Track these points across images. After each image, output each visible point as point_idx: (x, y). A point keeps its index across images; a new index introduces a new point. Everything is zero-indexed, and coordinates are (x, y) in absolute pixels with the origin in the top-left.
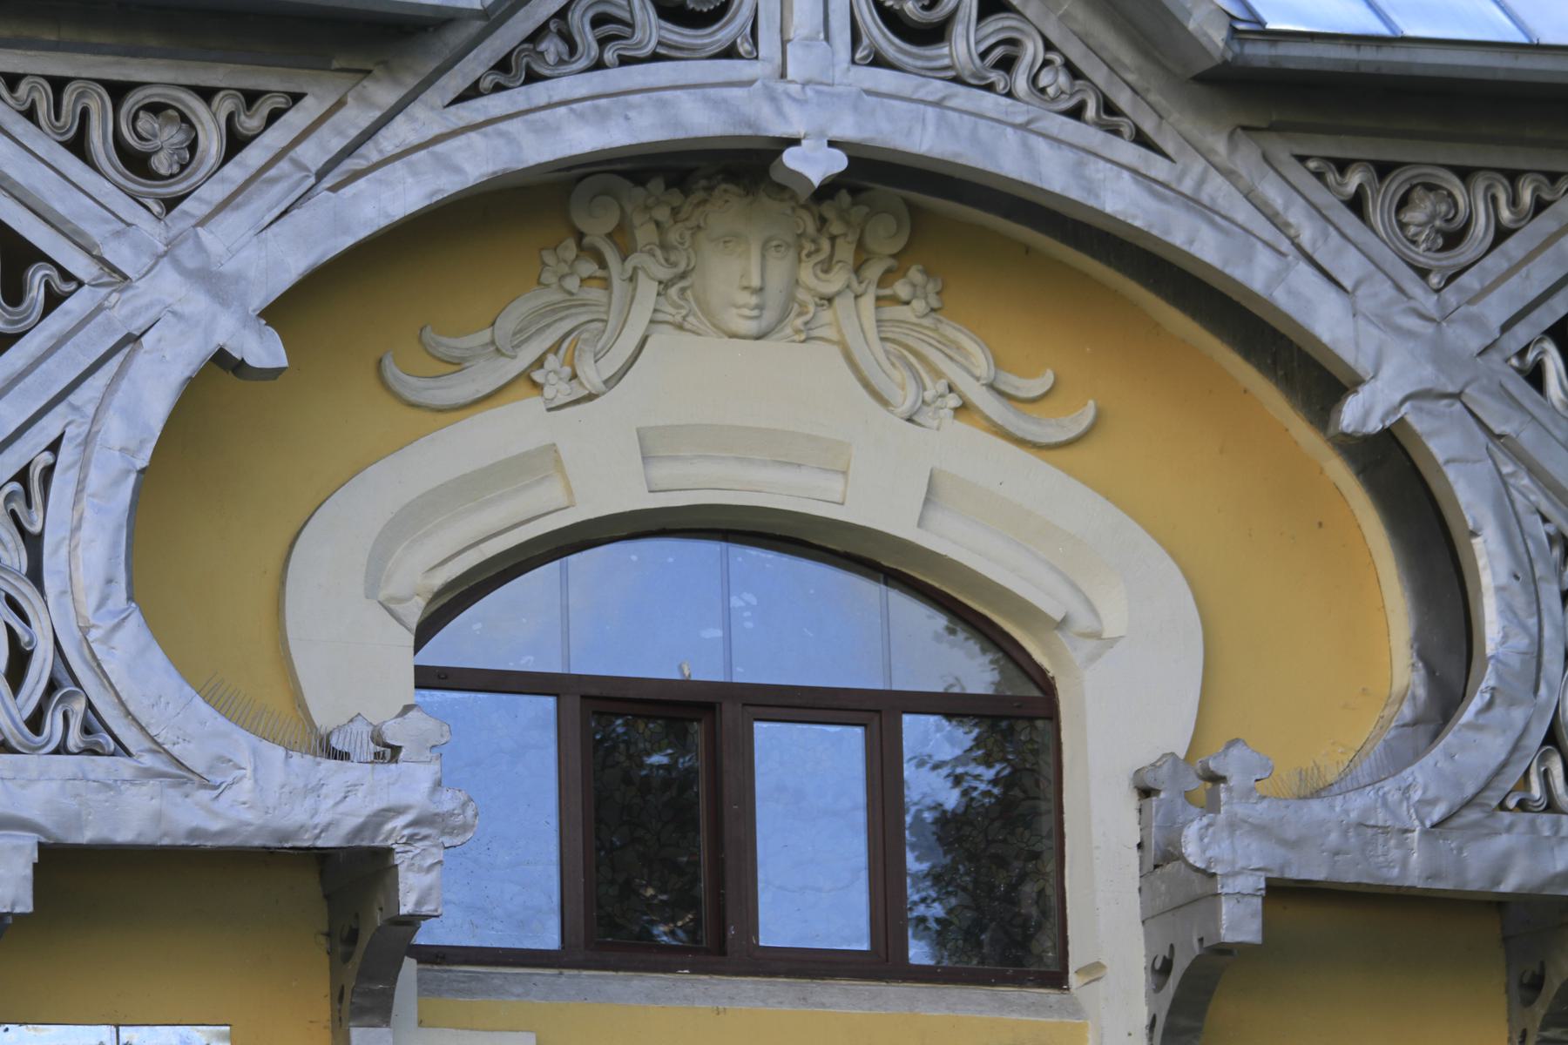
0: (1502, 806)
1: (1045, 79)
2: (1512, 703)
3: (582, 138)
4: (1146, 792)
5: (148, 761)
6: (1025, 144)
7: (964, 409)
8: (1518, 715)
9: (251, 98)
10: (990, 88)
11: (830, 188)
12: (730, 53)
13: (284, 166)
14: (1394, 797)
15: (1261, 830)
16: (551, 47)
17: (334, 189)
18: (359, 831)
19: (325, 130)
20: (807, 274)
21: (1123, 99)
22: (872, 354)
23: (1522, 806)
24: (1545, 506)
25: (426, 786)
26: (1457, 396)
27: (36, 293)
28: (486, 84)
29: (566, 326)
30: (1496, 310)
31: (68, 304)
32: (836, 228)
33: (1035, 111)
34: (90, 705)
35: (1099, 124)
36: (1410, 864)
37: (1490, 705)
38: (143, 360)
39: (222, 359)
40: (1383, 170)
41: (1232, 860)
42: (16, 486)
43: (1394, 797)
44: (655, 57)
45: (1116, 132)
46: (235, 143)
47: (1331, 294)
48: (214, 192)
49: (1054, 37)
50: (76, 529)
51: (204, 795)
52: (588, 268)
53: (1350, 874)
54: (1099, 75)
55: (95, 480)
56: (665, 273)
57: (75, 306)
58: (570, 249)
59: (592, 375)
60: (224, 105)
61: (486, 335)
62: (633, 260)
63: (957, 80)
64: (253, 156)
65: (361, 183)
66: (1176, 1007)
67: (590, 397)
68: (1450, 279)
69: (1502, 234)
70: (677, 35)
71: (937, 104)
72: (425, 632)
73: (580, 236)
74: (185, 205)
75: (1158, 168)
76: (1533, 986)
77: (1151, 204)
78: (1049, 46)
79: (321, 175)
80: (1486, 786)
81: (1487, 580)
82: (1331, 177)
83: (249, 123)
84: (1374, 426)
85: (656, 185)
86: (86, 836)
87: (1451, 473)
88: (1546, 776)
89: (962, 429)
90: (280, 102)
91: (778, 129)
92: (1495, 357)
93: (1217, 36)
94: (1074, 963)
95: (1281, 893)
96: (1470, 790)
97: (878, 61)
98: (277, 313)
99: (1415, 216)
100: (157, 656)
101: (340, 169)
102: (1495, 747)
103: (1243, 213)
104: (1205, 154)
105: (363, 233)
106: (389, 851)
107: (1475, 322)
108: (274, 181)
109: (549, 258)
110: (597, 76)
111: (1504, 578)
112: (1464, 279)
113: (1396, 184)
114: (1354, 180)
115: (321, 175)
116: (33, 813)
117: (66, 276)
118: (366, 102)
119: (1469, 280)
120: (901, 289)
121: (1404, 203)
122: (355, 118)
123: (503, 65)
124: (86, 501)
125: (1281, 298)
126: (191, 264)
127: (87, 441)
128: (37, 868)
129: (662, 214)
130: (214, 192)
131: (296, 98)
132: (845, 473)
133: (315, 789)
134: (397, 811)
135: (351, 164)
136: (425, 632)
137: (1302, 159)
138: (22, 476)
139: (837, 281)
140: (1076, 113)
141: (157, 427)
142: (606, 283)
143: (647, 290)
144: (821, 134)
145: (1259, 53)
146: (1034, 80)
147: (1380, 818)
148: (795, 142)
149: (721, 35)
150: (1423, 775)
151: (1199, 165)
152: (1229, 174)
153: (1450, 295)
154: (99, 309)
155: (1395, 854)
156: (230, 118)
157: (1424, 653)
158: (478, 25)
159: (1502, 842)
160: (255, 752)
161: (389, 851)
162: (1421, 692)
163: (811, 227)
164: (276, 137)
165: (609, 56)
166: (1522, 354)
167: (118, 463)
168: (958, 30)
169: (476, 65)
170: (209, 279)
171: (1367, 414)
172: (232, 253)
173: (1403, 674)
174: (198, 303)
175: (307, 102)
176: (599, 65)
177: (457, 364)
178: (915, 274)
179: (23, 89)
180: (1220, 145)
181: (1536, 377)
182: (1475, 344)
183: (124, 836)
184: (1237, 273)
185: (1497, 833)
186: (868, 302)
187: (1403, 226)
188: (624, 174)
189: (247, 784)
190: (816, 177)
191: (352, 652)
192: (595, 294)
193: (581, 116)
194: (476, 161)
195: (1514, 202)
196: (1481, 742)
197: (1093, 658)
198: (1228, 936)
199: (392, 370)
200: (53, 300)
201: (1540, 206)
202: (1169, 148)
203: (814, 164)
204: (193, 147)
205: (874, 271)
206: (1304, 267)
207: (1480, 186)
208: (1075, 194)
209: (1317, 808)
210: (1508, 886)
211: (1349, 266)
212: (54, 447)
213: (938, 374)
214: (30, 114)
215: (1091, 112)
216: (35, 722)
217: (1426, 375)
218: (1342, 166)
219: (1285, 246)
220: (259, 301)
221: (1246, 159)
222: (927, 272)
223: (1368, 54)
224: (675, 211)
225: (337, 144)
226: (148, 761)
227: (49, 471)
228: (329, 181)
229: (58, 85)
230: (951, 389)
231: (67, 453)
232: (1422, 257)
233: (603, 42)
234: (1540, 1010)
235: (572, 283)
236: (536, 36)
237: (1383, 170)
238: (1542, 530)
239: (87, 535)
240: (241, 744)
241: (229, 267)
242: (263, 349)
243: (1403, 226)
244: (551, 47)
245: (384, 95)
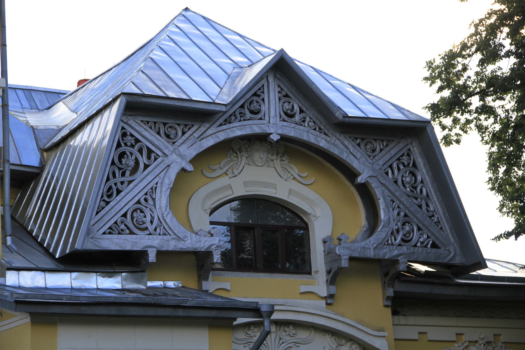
0: (385, 244)
1: (310, 124)
2: (386, 227)
3: (238, 133)
4: (325, 242)
5: (173, 236)
6: (308, 134)
7: (294, 178)
8: (387, 229)
9: (186, 126)
10: (301, 125)
11: (278, 141)
12: (261, 119)
13: (192, 137)
14: (368, 243)
15: (348, 248)
16: (233, 118)
17: (200, 141)
18: (207, 248)
19: (198, 131)
20: (269, 156)
21: (322, 127)
22: (279, 169)
23: (388, 244)
24: (390, 195)
25: (217, 241)
26: (376, 177)
27: (153, 158)
28: (223, 123)
29: (231, 164)
30: (381, 162)
31: (158, 160)
32: (274, 149)
33: (309, 129)
34: (164, 228)
35: (318, 131)
36: (371, 254)
37: (382, 228)
38: (170, 170)
39: (183, 170)
40: (363, 139)
41: (344, 253)
42: (151, 190)
43: (368, 243)
44: (249, 120)
45: (321, 133)
46: (184, 133)
47: (356, 160)
48: (180, 141)
49: (311, 117)
50: (161, 197)
51: (183, 242)
52: (235, 155)
53: (362, 256)
54: (318, 123)
55: (164, 189)
56: (247, 156)
57: (159, 160)
58: (231, 151)
59: (236, 172)
60: (182, 127)
61: (219, 166)
62: (242, 153)
63: (296, 124)
64: (187, 135)
65: (204, 140)
66: (332, 278)
67: (235, 176)
68: (374, 157)
69: (381, 150)
70: (252, 116)
71: (294, 128)
72: (211, 213)
73: (233, 149)
74: (176, 143)
75: (328, 139)
76: (386, 275)
77: (328, 145)
78: (311, 118)
79: (198, 138)
80: (382, 241)
81: (381, 207)
82: (355, 140)
83: (186, 130)
84: (363, 182)
85: (246, 141)
86: (164, 249)
87: (375, 189)
88: (391, 239)
89: (294, 182)
90: (190, 126)
91: (269, 132)
92: (381, 170)
93: (341, 117)
94: (313, 270)
95: (352, 259)
96: (380, 242)
97: (284, 120)
98: (192, 161)
99: (368, 147)
100: (175, 219)
101: (201, 138)
102: (383, 235)
103: (342, 146)
104: (335, 136)
105: (205, 148)
106: (212, 252)
107: (378, 164)
108: (190, 139)
109: (228, 153)
110: (240, 122)
111: (384, 207)
112: (376, 157)
113: (365, 142)
114: (358, 141)
115: (198, 138)
116: (155, 245)
117: (158, 155)
118: (204, 126)
119: (377, 158)
120: (284, 159)
121: (366, 145)
122: (203, 129)
123: (225, 121)
124: (162, 193)
125: (348, 160)
126: (178, 153)
127: (162, 183)
128: (156, 254)
129: (247, 146)
130: (180, 141)
131: (193, 126)
132: (276, 189)
133: (200, 241)
134: (213, 245)
135: (202, 137)
136: (211, 213)
137: (350, 137)
138: (152, 188)
139: (274, 157)
140: (315, 129)
141: (173, 180)
142: (237, 157)
143: (244, 158)
144: (276, 132)
145: (347, 120)
146: (308, 124)
147: (366, 246)
148: (272, 134)
149: (259, 116)
150: (372, 239)
151: (335, 138)
152: (339, 140)
153: (374, 160)
154: (163, 161)
155: (369, 252)
156: (183, 129)
157: (368, 219)
158: (222, 114)
159: (385, 250)
160: (191, 235)
161: (212, 252)
162: (367, 226)
163: (270, 148)
164: (190, 132)
165: (242, 119)
166: (385, 170)
167: (167, 186)
168: (296, 116)
169: (221, 121)
170: (180, 156)
171: (362, 179)
172: (184, 151)
173: (363, 221)
174: (179, 160)
175: (195, 126)
176: (240, 121)
177: (214, 170)
178: (286, 156)
179: (150, 124)
180: (338, 135)
181: (387, 173)
182: (378, 168)
183: (170, 249)
184: (341, 156)
185: (384, 249)
186: (279, 161)
187: (366, 149)
188: (240, 139)
189: (189, 240)
190: (275, 139)
191: (200, 219)
192: (236, 159)
193: (238, 129)
194: (222, 136)
195: (383, 145)
196: (381, 233)
197: (316, 220)
198: (343, 266)
199: (204, 172)
200: (156, 159)
201: (387, 146)
202: (330, 136)
203: (275, 137)
204: (177, 134)
205: (280, 156)
206: (351, 155)
207: (378, 142)
208: (316, 143)
209: (356, 245)
210: (386, 258)
211: (358, 155)
212: (157, 184)
213: (290, 173)
214: (151, 128)
215: (317, 129)
216: (155, 229)
217: (371, 173)
218: (356, 139)
219: (348, 152)
220: (188, 159)
221: (342, 138)
222: (287, 156)
223: (364, 120)
224: (249, 146)
225: (200, 134)
226: (173, 236)
227: (156, 188)
228: (199, 139)
229: (155, 123)
230: (292, 175)
231: (159, 185)
232: (369, 153)
233: (241, 117)
234: (388, 278)
235: (232, 157)
236: (230, 116)
237: (363, 139)
238: (389, 199)
239: (162, 199)
240: (188, 234)
241: (184, 154)
242: (190, 168)
243: (366, 149)
244: (233, 118)
245: (207, 125)
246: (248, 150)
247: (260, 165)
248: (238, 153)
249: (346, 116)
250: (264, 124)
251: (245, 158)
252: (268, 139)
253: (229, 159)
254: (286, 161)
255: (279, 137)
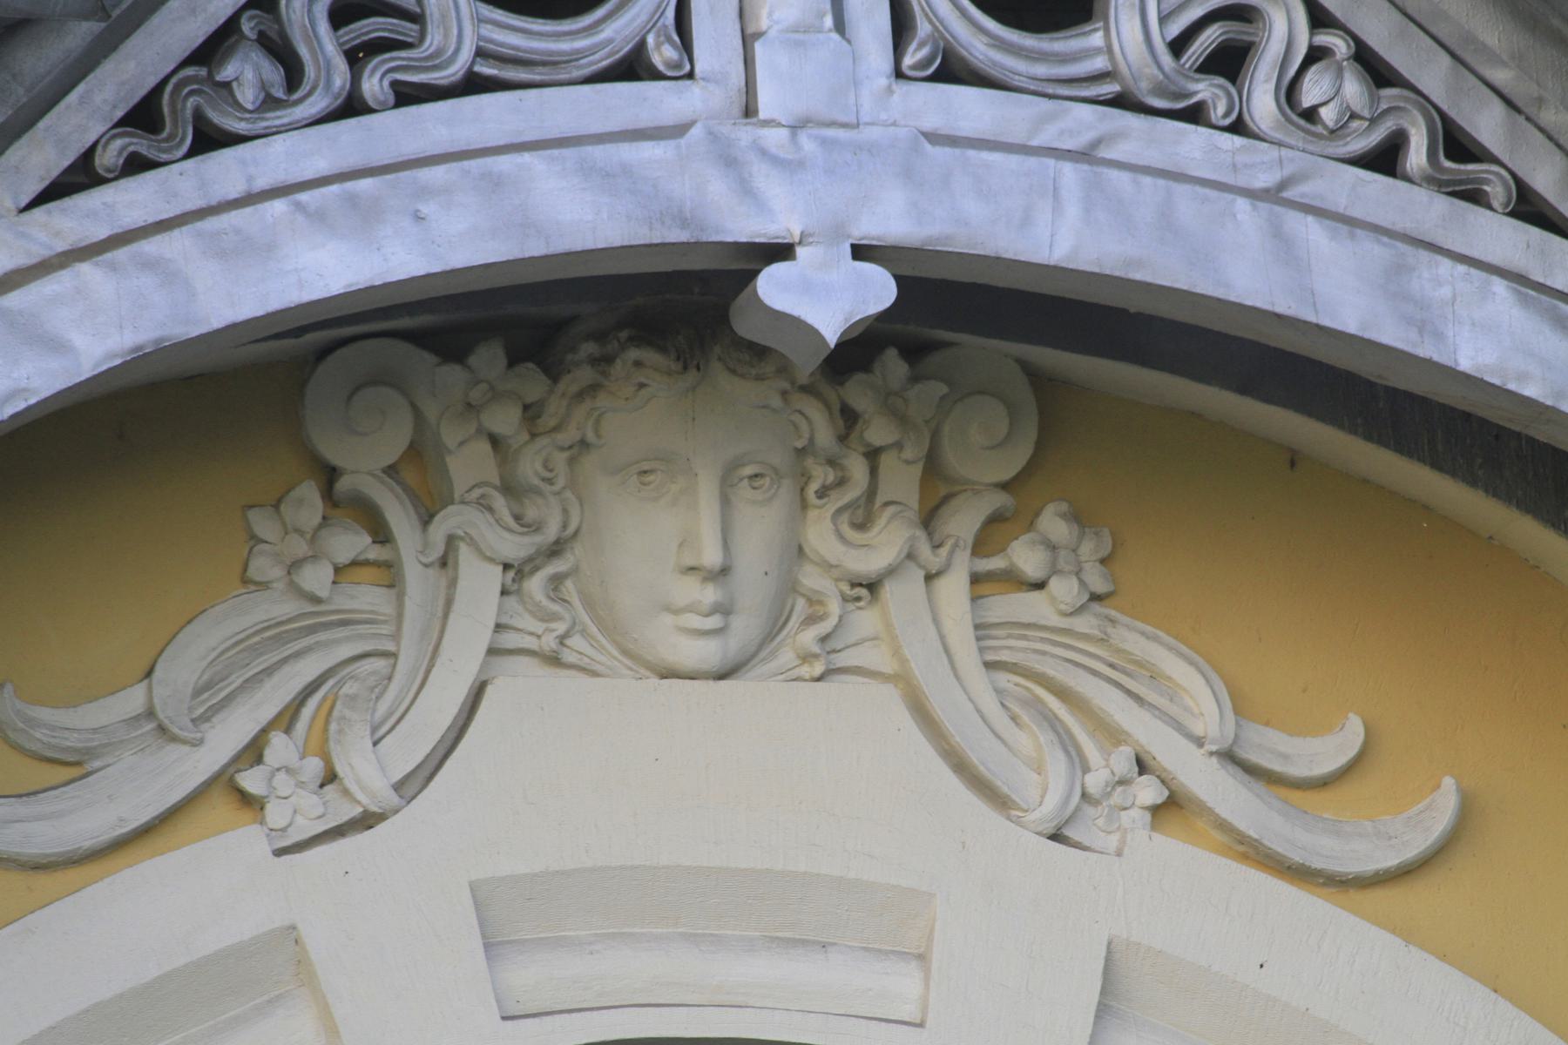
1: (1313, 90)
3: (322, 264)
7: (1173, 807)
10: (1194, 114)
11: (859, 350)
16: (247, 71)
21: (1486, 124)
22: (970, 701)
28: (109, 157)
32: (878, 432)
33: (1294, 161)
35: (1437, 182)
44: (473, 84)
45: (1474, 196)
52: (350, 543)
54: (1430, 73)
56: (515, 547)
58: (308, 503)
63: (1123, 102)
67: (366, 821)
71: (1084, 156)
73: (329, 475)
85: (489, 358)
89: (1171, 852)
91: (744, 226)
97: (951, 69)
109: (263, 524)
120: (1026, 557)
123: (144, 116)
129: (504, 420)
132: (922, 958)
140: (1386, 159)
142: (390, 574)
143: (479, 583)
144: (837, 231)
146: (1290, 93)
148: (781, 252)
165: (373, 85)
176: (352, 107)
177: (75, 764)
178: (1053, 524)
186: (954, 587)
192: (366, 597)
193: (318, 217)
203: (825, 297)
205: (964, 521)
208: (1390, 334)
213: (1112, 735)
215: (1416, 156)
222: (1079, 518)
224: (531, 413)
233: (357, 57)
235: (316, 578)
236: (211, 51)
244: (247, 71)
246: (529, 467)
247: (705, 653)
248: (399, 517)
249: (663, 350)
250: (678, 130)
251: (495, 576)
252: (745, 326)
253: (277, 607)
254: (1064, 589)
255: (877, 291)
